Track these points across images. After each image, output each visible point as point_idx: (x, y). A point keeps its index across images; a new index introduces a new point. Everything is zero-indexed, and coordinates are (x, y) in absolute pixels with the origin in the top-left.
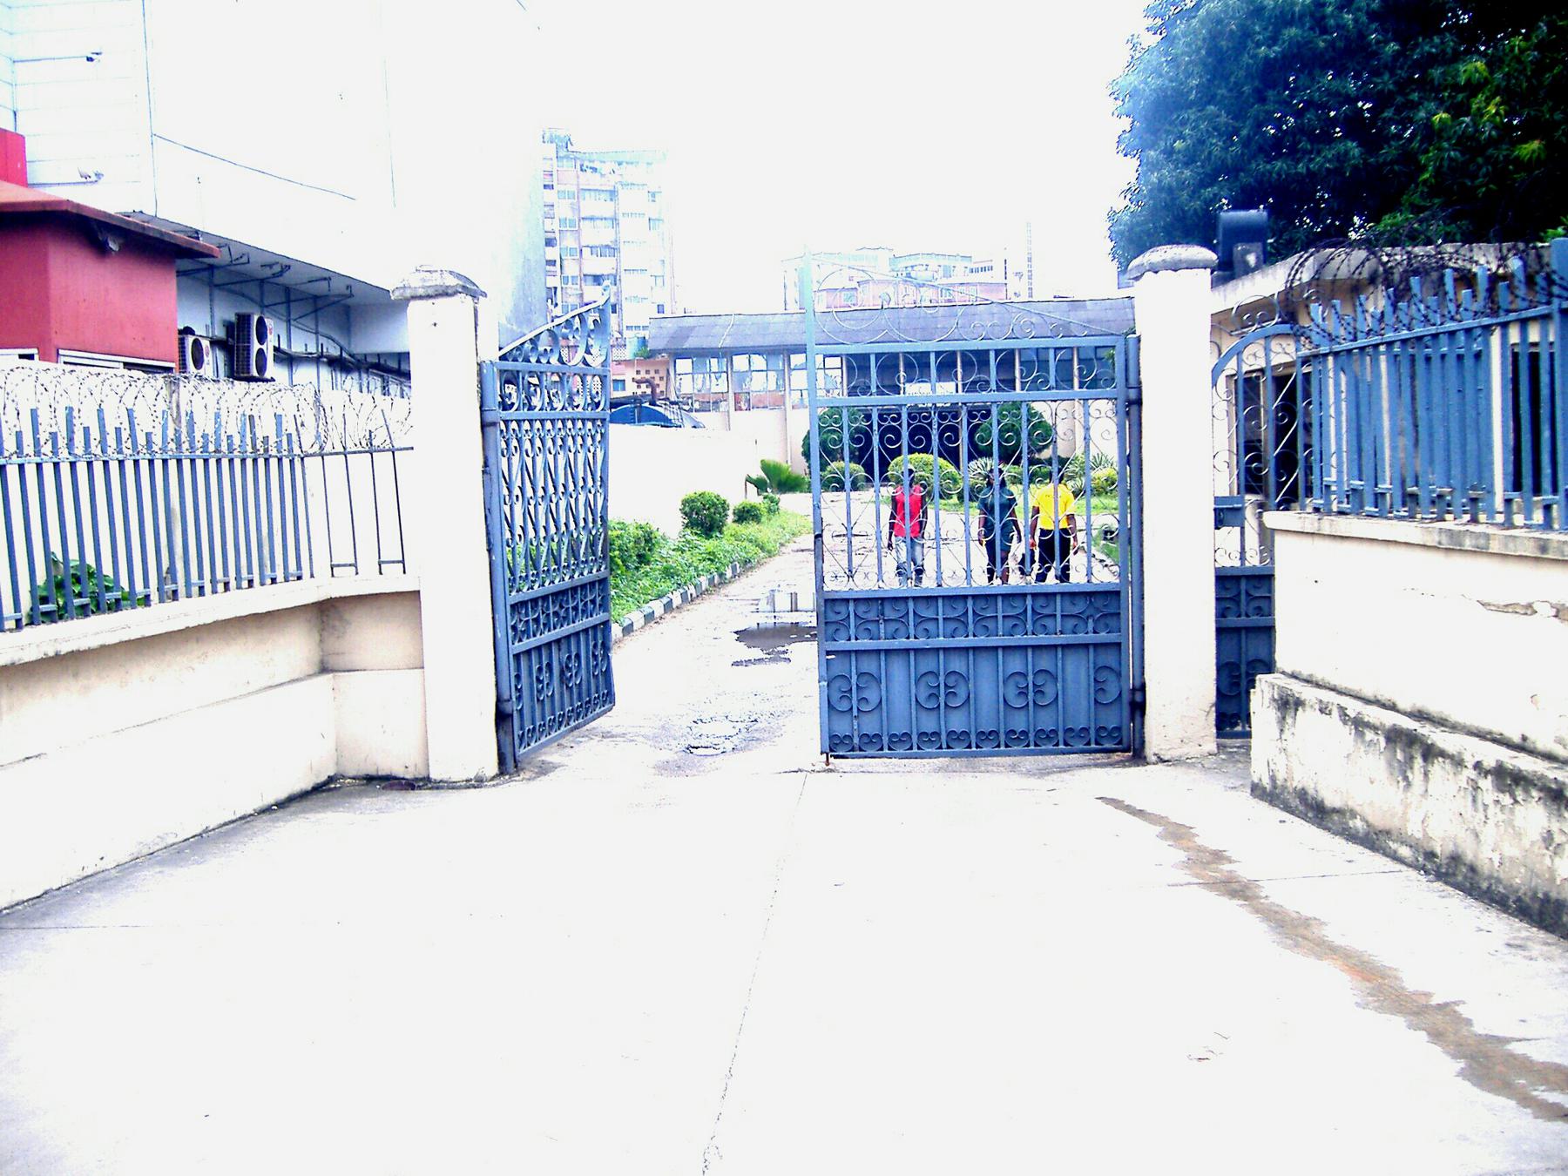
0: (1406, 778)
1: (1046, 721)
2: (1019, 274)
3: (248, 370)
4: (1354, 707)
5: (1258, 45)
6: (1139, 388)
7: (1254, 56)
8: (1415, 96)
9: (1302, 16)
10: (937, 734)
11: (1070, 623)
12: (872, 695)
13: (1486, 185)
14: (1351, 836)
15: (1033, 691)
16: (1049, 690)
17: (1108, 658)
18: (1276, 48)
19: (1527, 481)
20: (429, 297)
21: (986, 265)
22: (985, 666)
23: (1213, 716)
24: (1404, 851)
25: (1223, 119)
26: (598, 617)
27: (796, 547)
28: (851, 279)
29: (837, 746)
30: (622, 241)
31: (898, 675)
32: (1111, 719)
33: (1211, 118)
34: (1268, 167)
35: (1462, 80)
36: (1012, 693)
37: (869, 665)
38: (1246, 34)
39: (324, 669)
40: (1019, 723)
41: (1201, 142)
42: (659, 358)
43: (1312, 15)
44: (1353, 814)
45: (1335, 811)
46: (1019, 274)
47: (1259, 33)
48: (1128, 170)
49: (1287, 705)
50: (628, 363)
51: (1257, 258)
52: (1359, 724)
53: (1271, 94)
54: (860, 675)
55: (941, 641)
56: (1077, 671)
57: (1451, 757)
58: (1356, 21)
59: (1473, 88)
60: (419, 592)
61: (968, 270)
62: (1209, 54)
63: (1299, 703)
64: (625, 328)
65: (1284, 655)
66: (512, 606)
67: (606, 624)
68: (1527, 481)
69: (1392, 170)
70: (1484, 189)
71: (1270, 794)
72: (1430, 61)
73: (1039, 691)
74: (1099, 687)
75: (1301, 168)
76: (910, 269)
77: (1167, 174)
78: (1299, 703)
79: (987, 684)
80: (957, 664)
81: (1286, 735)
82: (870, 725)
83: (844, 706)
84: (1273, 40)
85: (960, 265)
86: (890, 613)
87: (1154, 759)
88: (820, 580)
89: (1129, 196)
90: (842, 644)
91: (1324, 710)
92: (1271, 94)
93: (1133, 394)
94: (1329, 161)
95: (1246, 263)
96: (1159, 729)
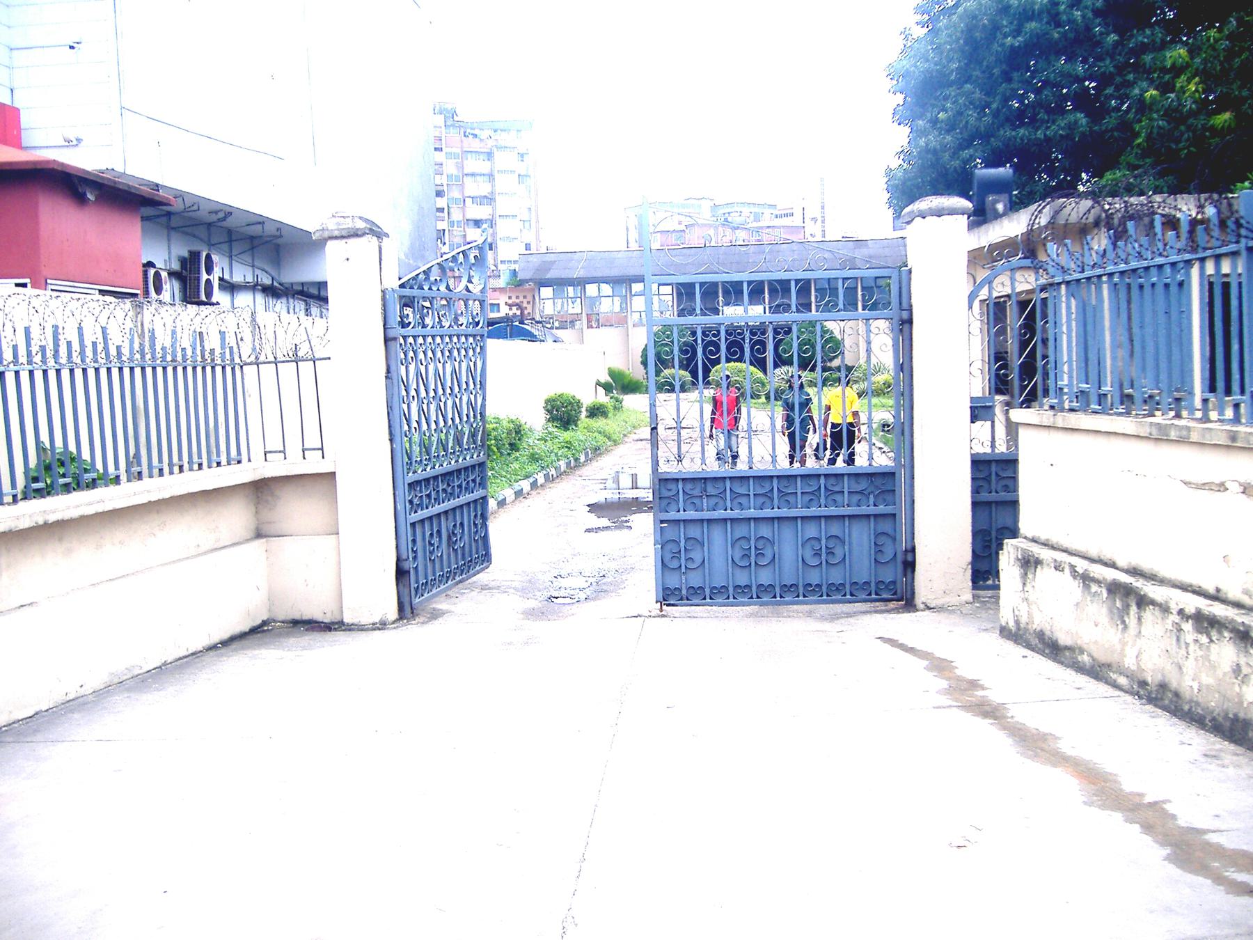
0: (1123, 622)
1: (836, 576)
2: (815, 220)
3: (198, 295)
4: (1081, 565)
5: (1005, 36)
6: (910, 310)
7: (1003, 45)
8: (1131, 77)
9: (1040, 13)
10: (749, 587)
11: (855, 498)
12: (697, 555)
13: (1187, 148)
14: (1080, 669)
15: (825, 553)
16: (839, 552)
17: (885, 526)
18: (1020, 39)
19: (1220, 384)
20: (343, 237)
21: (788, 211)
22: (787, 532)
23: (969, 572)
24: (1122, 681)
25: (978, 94)
26: (478, 494)
27: (636, 437)
28: (680, 223)
29: (669, 596)
30: (497, 193)
31: (718, 539)
32: (888, 575)
33: (968, 95)
34: (1014, 133)
35: (1169, 64)
36: (808, 554)
37: (694, 532)
38: (996, 28)
39: (259, 535)
40: (814, 577)
41: (960, 113)
42: (527, 286)
43: (1049, 12)
44: (1082, 651)
45: (1067, 648)
46: (815, 220)
47: (1006, 26)
48: (901, 136)
49: (1029, 563)
50: (502, 290)
51: (1005, 206)
52: (1086, 579)
53: (1016, 75)
54: (687, 539)
55: (752, 513)
56: (860, 537)
57: (1160, 605)
58: (1083, 17)
59: (1177, 70)
60: (333, 474)
61: (773, 216)
62: (966, 43)
63: (1038, 562)
64: (499, 262)
65: (1026, 524)
66: (409, 484)
67: (484, 498)
68: (1220, 384)
69: (1112, 136)
70: (1186, 151)
71: (1015, 635)
72: (1143, 48)
73: (830, 553)
74: (879, 549)
75: (1040, 134)
76: (727, 215)
77: (933, 140)
78: (1038, 562)
79: (789, 547)
80: (765, 531)
81: (1028, 587)
82: (695, 580)
83: (675, 564)
84: (1017, 32)
85: (767, 212)
86: (711, 490)
87: (922, 606)
88: (655, 464)
89: (902, 157)
90: (673, 515)
91: (1058, 567)
92: (1016, 75)
93: (905, 315)
94: (1062, 129)
95: (995, 210)
96: (926, 582)
